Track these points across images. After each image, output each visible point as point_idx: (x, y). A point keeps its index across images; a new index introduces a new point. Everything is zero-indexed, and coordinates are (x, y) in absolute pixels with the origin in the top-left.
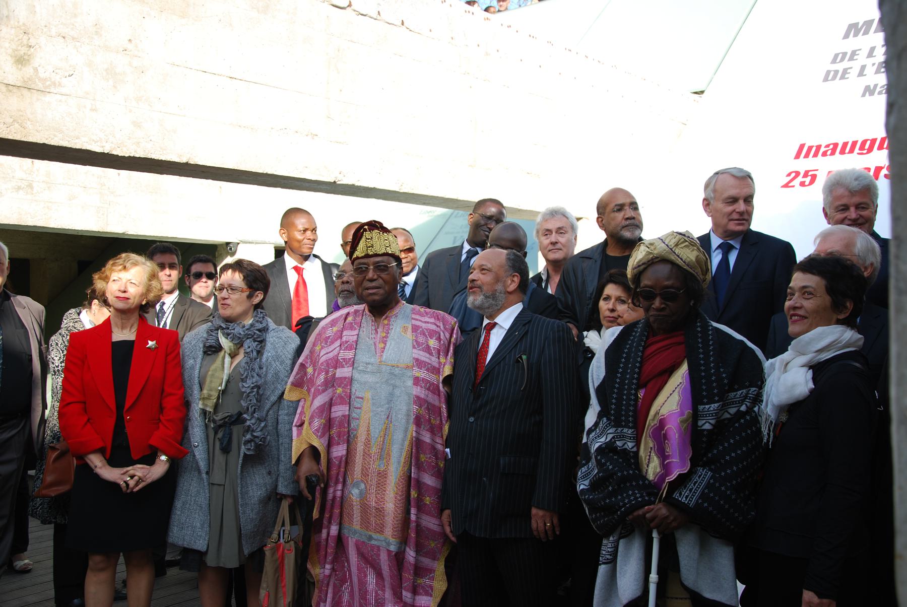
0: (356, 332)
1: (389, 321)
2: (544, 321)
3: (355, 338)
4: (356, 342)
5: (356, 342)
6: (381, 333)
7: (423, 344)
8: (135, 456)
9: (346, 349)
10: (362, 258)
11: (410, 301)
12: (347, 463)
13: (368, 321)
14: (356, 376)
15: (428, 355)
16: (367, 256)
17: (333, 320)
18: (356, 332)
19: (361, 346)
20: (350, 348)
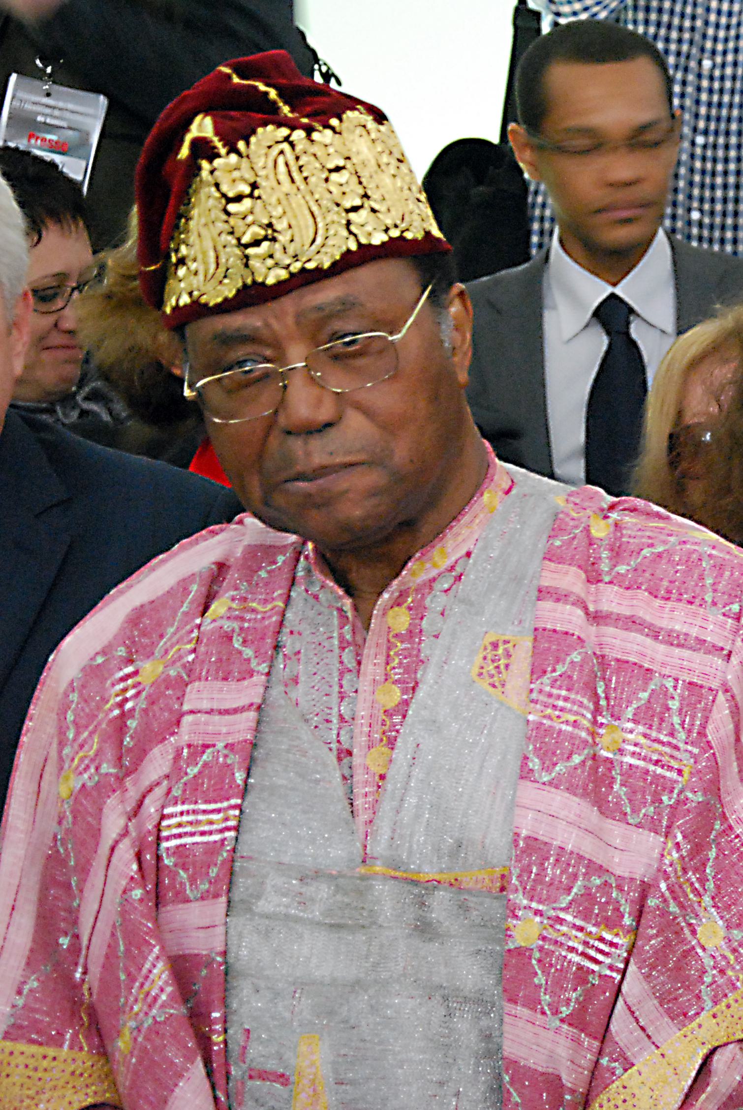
0: (249, 692)
1: (418, 612)
2: (95, 117)
3: (241, 727)
4: (250, 753)
5: (250, 753)
6: (374, 693)
7: (578, 745)
8: (537, 26)
9: (193, 792)
10: (226, 307)
11: (661, 682)
12: (226, 1051)
13: (316, 608)
14: (245, 952)
15: (592, 814)
16: (253, 295)
17: (136, 618)
18: (249, 692)
19: (272, 774)
20: (214, 786)
